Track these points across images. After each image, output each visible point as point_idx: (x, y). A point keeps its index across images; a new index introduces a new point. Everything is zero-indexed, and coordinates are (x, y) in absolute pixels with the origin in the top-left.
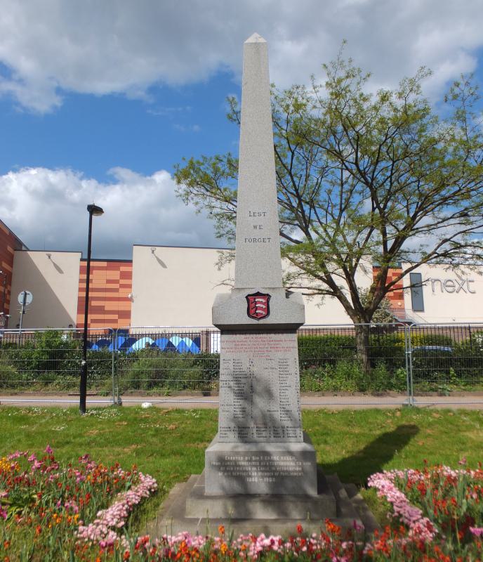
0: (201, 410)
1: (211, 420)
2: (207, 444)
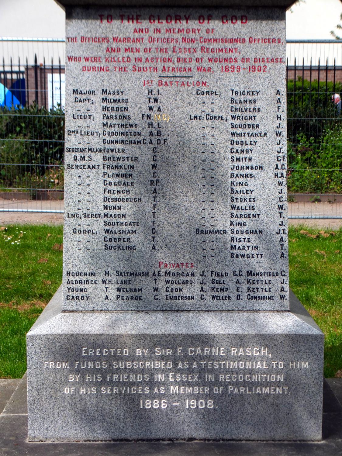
0: (26, 229)
1: (48, 249)
2: (39, 304)
